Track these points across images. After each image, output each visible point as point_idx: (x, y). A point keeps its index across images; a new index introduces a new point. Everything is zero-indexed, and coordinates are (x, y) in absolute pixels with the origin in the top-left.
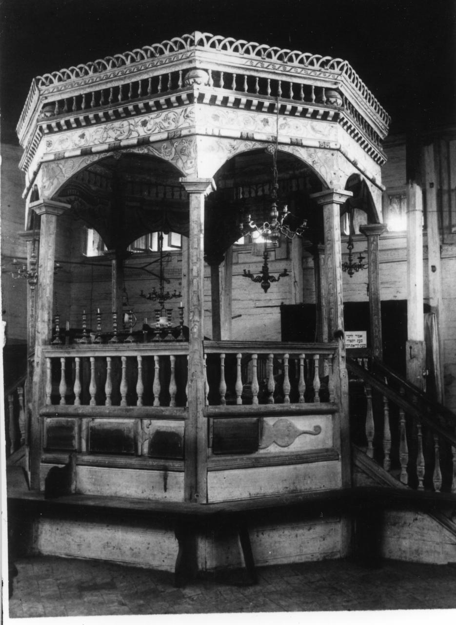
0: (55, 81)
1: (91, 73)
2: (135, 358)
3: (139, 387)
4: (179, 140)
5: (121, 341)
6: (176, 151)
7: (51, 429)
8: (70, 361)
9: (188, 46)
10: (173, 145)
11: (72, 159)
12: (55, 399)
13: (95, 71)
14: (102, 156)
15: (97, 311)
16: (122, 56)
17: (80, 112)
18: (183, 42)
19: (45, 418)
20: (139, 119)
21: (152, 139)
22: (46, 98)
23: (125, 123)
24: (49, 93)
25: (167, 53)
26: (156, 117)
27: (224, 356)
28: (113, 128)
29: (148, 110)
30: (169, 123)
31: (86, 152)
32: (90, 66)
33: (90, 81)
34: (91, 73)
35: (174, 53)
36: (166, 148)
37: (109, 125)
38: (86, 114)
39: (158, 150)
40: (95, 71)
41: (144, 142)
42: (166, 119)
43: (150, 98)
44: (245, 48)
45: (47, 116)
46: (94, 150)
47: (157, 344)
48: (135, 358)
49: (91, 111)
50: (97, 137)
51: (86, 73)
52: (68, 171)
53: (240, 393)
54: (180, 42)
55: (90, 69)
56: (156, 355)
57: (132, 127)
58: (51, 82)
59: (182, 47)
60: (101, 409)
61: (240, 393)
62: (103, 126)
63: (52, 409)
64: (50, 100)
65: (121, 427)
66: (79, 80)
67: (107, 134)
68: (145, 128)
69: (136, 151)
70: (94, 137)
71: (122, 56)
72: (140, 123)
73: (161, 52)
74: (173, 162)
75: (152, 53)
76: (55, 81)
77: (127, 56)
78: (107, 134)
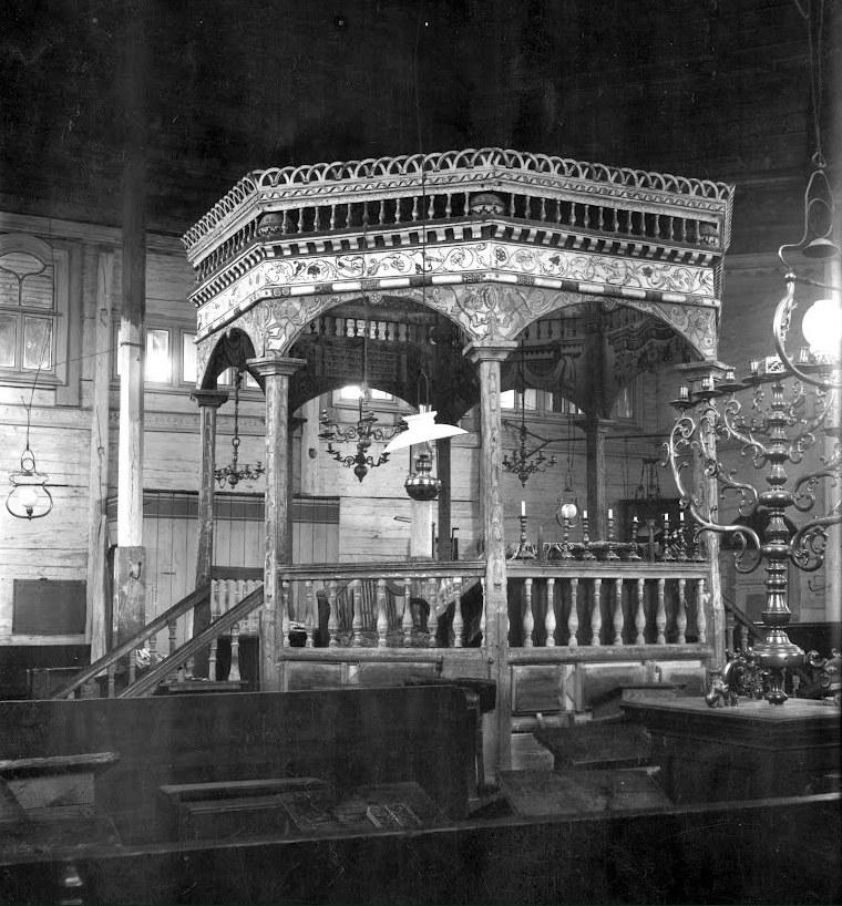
0: (524, 167)
1: (582, 177)
2: (636, 581)
3: (574, 621)
4: (695, 309)
5: (624, 559)
6: (690, 322)
7: (525, 683)
8: (652, 584)
9: (556, 173)
10: (686, 312)
11: (546, 291)
12: (517, 637)
13: (589, 176)
14: (588, 298)
15: (607, 514)
16: (634, 173)
17: (564, 226)
18: (716, 190)
19: (514, 667)
20: (640, 264)
21: (665, 297)
22: (500, 184)
23: (620, 263)
24: (511, 180)
25: (692, 193)
26: (664, 269)
27: (683, 583)
28: (602, 264)
29: (658, 255)
30: (681, 283)
31: (569, 287)
32: (584, 167)
33: (579, 188)
34: (582, 177)
35: (701, 198)
36: (678, 314)
37: (597, 257)
38: (573, 234)
39: (668, 313)
40: (589, 176)
41: (654, 298)
42: (677, 276)
43: (669, 244)
44: (390, 166)
45: (496, 212)
46: (581, 287)
47: (672, 564)
48: (636, 581)
49: (582, 232)
50: (591, 272)
51: (575, 174)
52: (540, 308)
53: (573, 632)
54: (713, 189)
55: (583, 171)
56: (620, 577)
57: (629, 271)
58: (517, 165)
59: (712, 194)
60: (609, 650)
61: (573, 632)
62: (588, 257)
63: (513, 655)
64: (505, 189)
65: (631, 672)
66: (562, 179)
67: (594, 270)
68: (650, 280)
69: (635, 305)
70: (575, 268)
71: (519, 155)
72: (641, 270)
73: (686, 191)
74: (687, 335)
75: (532, 162)
76: (524, 167)
77: (693, 184)
78: (594, 270)
